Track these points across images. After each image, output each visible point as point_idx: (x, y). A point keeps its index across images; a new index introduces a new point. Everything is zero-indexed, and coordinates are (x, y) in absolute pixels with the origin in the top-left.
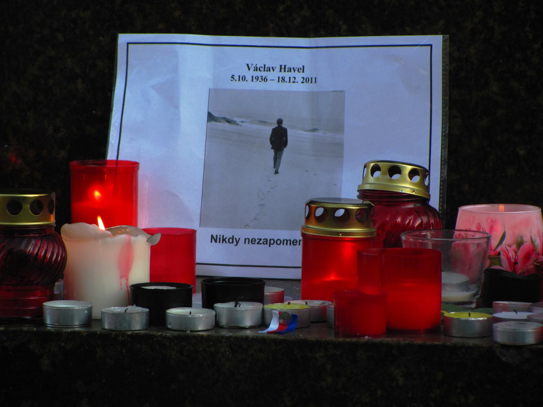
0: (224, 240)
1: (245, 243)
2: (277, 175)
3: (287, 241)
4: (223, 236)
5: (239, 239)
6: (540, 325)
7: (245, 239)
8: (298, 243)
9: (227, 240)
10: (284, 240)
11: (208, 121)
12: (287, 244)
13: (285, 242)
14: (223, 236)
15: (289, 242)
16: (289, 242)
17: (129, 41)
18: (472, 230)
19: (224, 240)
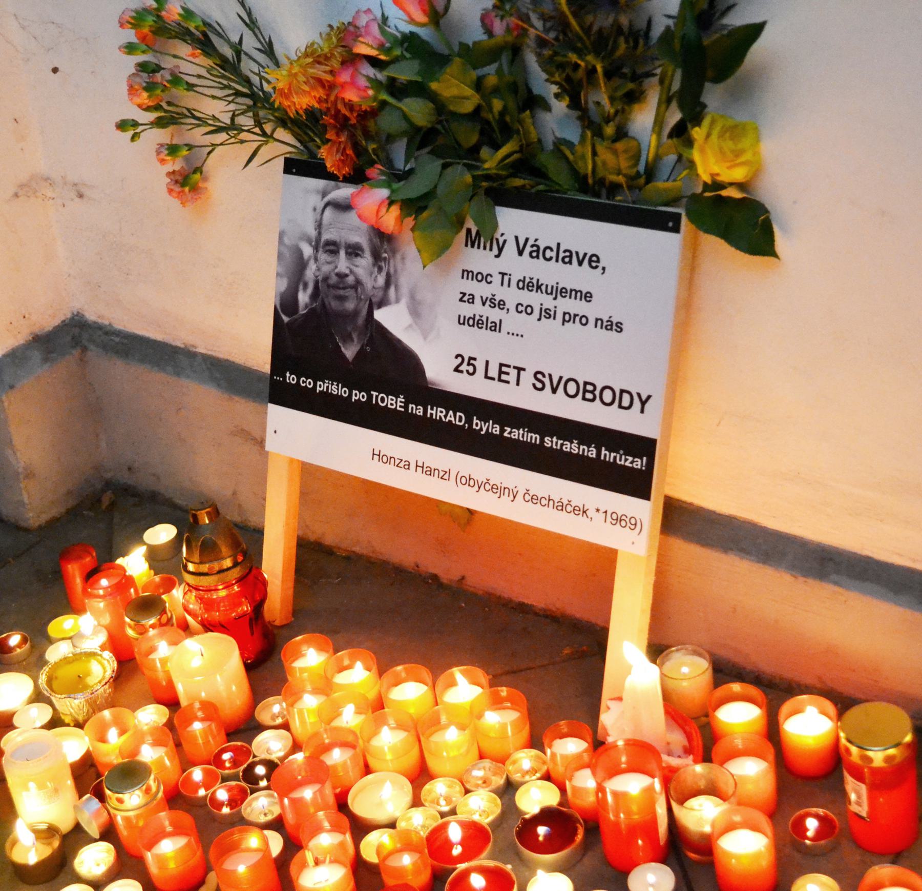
0: (539, 287)
1: (596, 326)
2: (52, 74)
3: (576, 292)
4: (538, 280)
5: (649, 397)
6: (675, 20)
7: (597, 320)
8: (568, 295)
9: (543, 288)
10: (571, 291)
11: (292, 461)
12: (576, 298)
13: (573, 293)
14: (538, 280)
15: (579, 294)
16: (579, 294)
17: (588, 380)
18: (579, 865)
19: (539, 287)
